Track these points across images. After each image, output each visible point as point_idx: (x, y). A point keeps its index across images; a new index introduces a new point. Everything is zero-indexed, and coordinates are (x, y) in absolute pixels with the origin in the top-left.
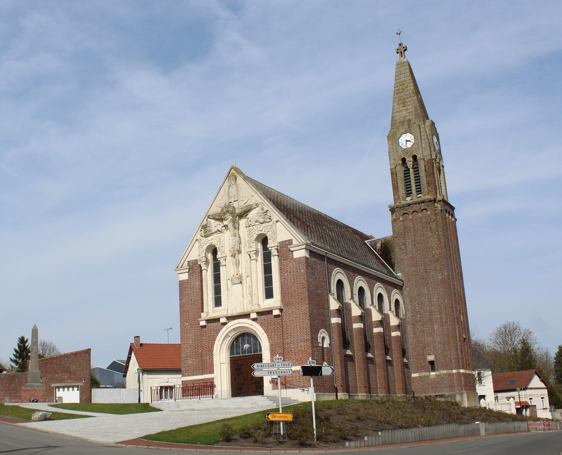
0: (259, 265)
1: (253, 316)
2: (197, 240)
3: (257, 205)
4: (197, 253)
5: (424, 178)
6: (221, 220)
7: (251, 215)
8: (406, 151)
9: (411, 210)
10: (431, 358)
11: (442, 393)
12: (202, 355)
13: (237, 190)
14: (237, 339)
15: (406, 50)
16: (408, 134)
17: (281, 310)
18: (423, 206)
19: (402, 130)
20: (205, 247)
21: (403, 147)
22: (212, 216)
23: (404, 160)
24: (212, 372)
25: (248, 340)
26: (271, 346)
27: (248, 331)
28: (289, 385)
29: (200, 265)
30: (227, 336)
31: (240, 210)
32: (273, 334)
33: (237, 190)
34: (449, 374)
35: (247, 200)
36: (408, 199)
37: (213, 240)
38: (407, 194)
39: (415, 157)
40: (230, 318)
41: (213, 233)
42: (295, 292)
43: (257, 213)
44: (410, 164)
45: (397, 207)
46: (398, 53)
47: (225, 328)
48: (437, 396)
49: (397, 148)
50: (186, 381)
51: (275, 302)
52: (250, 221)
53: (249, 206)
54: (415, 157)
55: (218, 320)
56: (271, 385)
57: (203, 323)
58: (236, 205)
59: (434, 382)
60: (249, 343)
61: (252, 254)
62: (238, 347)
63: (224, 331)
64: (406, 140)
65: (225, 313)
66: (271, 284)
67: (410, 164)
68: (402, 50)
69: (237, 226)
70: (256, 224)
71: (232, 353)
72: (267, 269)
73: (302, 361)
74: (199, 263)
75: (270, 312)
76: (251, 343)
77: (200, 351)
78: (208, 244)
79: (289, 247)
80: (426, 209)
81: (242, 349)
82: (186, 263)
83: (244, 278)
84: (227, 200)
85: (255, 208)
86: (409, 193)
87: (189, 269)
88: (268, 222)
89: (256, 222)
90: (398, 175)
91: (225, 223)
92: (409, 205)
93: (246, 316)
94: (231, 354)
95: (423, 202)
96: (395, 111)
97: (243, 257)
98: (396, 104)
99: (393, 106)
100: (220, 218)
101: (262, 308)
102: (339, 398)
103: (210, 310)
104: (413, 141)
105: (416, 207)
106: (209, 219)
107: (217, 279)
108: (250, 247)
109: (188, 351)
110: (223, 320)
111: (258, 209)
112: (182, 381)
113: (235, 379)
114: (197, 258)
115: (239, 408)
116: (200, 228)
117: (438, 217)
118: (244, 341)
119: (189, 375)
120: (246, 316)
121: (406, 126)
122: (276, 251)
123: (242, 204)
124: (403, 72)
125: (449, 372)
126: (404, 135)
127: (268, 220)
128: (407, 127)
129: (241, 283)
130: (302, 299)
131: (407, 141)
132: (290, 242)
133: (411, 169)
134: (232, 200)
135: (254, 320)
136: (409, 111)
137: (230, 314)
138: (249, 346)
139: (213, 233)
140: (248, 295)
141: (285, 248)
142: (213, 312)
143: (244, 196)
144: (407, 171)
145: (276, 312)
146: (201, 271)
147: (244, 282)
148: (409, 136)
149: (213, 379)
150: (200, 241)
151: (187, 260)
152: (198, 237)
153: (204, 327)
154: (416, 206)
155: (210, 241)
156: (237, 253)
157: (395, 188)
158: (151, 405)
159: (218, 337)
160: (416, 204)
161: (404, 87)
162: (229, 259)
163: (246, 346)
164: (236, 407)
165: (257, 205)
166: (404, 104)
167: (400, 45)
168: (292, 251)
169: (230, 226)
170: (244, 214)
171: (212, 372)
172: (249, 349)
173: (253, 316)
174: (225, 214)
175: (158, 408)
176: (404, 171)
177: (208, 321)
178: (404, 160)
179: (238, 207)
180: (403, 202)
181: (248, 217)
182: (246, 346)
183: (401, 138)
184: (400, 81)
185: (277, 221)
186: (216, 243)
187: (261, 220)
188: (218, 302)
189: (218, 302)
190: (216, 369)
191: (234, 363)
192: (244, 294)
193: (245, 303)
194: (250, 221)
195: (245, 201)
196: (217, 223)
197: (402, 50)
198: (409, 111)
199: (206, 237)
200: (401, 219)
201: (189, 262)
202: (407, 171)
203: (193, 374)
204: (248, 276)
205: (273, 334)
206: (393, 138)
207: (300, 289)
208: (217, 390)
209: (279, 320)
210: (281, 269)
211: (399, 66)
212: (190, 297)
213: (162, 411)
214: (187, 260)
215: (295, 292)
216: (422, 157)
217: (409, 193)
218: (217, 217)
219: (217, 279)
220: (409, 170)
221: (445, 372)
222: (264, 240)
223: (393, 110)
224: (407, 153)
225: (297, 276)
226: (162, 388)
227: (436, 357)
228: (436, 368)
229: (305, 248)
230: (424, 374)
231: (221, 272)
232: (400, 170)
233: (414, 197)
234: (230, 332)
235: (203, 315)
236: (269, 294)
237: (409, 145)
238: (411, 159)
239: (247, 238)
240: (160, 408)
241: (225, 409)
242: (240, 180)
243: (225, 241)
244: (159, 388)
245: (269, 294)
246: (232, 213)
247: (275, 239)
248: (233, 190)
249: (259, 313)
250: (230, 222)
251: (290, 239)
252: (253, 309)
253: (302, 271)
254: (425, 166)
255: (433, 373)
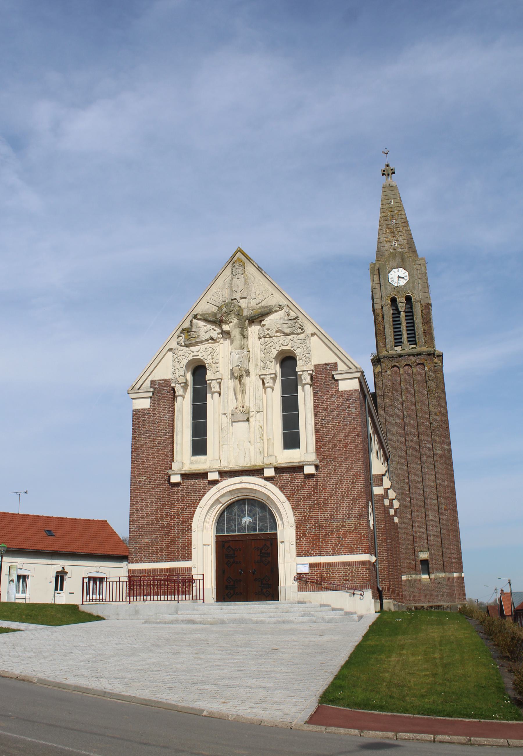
0: (275, 397)
1: (269, 472)
2: (170, 350)
3: (281, 307)
4: (171, 368)
5: (420, 325)
6: (219, 323)
7: (268, 321)
8: (397, 289)
9: (403, 363)
10: (424, 556)
11: (439, 604)
12: (169, 530)
13: (246, 282)
14: (229, 507)
15: (394, 173)
16: (401, 269)
17: (317, 467)
18: (419, 359)
19: (392, 263)
20: (185, 362)
21: (393, 283)
22: (202, 315)
23: (394, 301)
24: (188, 557)
25: (250, 511)
26: (298, 522)
27: (251, 495)
28: (326, 585)
29: (173, 389)
30: (217, 501)
31: (250, 313)
32: (301, 503)
33: (246, 282)
34: (449, 579)
35: (262, 298)
36: (398, 349)
37: (200, 352)
38: (396, 343)
39: (408, 299)
40: (225, 474)
41: (202, 342)
42: (340, 441)
43: (280, 319)
44: (402, 305)
45: (384, 357)
46: (383, 174)
47: (214, 489)
48: (431, 607)
49: (385, 285)
50: (136, 571)
51: (306, 454)
52: (268, 329)
53: (266, 307)
54: (408, 299)
55: (204, 475)
56: (296, 584)
57: (175, 479)
58: (243, 304)
59: (428, 588)
60: (252, 514)
61: (268, 379)
62: (231, 520)
63: (212, 494)
64: (398, 277)
65: (216, 465)
66: (296, 426)
67: (402, 305)
68: (388, 172)
69: (246, 333)
70: (278, 334)
71: (219, 529)
72: (290, 405)
73: (351, 548)
74: (173, 385)
75: (300, 468)
76: (254, 515)
77: (165, 523)
78: (190, 358)
79: (333, 373)
80: (422, 364)
81: (239, 524)
82: (148, 383)
83: (251, 414)
84: (228, 296)
85: (276, 311)
86: (398, 342)
87: (154, 392)
88: (298, 334)
89: (277, 332)
90: (385, 317)
91: (226, 328)
92: (400, 356)
93: (257, 472)
94: (218, 531)
95: (420, 354)
96: (382, 240)
97: (252, 383)
98: (383, 232)
99: (379, 234)
100: (216, 320)
101: (279, 462)
102: (385, 607)
103: (184, 460)
104: (407, 278)
105: (410, 360)
106: (195, 321)
107: (199, 413)
108: (265, 367)
109: (144, 522)
110: (213, 476)
111: (281, 314)
112: (130, 571)
113: (224, 572)
114: (169, 376)
115: (284, 622)
116: (178, 332)
117: (438, 375)
118: (242, 511)
119: (142, 561)
120: (257, 472)
121: (398, 259)
122: (309, 378)
123: (253, 303)
124: (392, 197)
125: (448, 575)
126: (395, 270)
127: (299, 331)
128: (400, 260)
129: (248, 420)
130: (352, 453)
131: (399, 277)
132: (334, 366)
133: (402, 313)
134: (238, 296)
135: (269, 479)
136: (400, 243)
137: (226, 466)
138: (251, 520)
139: (202, 342)
140: (258, 440)
141: (324, 376)
142: (191, 463)
143: (257, 293)
144: (397, 312)
145: (309, 470)
146: (174, 397)
147: (251, 420)
148: (402, 272)
149: (189, 569)
150: (176, 352)
151: (150, 379)
152: (173, 344)
153: (177, 484)
154: (409, 358)
155: (195, 354)
156: (244, 373)
157: (380, 333)
158: (82, 608)
159: (202, 503)
160: (409, 355)
161: (393, 214)
162: (229, 384)
163: (247, 520)
164: (280, 619)
165: (281, 307)
166: (394, 234)
167: (388, 166)
168: (337, 380)
169: (236, 333)
170: (257, 318)
171: (188, 557)
172: (252, 525)
173: (269, 472)
174: (228, 313)
175: (95, 613)
176: (393, 314)
177: (185, 476)
178: (394, 301)
179: (247, 306)
180: (392, 352)
181: (263, 322)
182: (247, 520)
183: (391, 273)
184: (387, 206)
185: (313, 335)
186: (205, 357)
187: (287, 330)
188: (199, 447)
189: (199, 447)
190: (194, 553)
191: (224, 546)
192: (246, 436)
193: (253, 453)
194: (268, 329)
195: (258, 300)
196: (210, 327)
197: (388, 172)
198: (400, 243)
199: (187, 346)
200: (389, 372)
201: (153, 383)
202: (397, 312)
203: (151, 560)
204: (258, 412)
205: (301, 503)
206: (379, 272)
207: (349, 439)
208: (196, 587)
209: (311, 482)
210: (316, 405)
211: (386, 189)
212: (150, 435)
213: (102, 619)
214: (150, 379)
215: (340, 441)
216: (418, 299)
217: (398, 342)
218: (212, 319)
219: (199, 413)
220: (399, 313)
221: (443, 575)
222: (287, 361)
223: (379, 238)
224: (399, 292)
225: (344, 418)
226: (90, 578)
227: (431, 555)
228: (431, 569)
229: (359, 378)
230: (414, 577)
231: (208, 403)
232: (388, 312)
233: (409, 348)
234: (223, 496)
235: (175, 466)
236: (291, 441)
237: (402, 283)
238: (403, 300)
239: (261, 355)
240: (100, 615)
241: (257, 622)
242: (250, 269)
243: (221, 358)
244: (86, 580)
245: (291, 441)
246: (239, 315)
247: (308, 360)
248: (239, 282)
249: (277, 470)
250: (235, 327)
251: (333, 362)
252: (267, 462)
253: (353, 410)
254: (422, 311)
255: (425, 577)
